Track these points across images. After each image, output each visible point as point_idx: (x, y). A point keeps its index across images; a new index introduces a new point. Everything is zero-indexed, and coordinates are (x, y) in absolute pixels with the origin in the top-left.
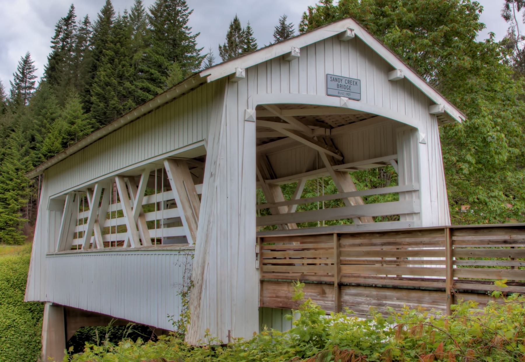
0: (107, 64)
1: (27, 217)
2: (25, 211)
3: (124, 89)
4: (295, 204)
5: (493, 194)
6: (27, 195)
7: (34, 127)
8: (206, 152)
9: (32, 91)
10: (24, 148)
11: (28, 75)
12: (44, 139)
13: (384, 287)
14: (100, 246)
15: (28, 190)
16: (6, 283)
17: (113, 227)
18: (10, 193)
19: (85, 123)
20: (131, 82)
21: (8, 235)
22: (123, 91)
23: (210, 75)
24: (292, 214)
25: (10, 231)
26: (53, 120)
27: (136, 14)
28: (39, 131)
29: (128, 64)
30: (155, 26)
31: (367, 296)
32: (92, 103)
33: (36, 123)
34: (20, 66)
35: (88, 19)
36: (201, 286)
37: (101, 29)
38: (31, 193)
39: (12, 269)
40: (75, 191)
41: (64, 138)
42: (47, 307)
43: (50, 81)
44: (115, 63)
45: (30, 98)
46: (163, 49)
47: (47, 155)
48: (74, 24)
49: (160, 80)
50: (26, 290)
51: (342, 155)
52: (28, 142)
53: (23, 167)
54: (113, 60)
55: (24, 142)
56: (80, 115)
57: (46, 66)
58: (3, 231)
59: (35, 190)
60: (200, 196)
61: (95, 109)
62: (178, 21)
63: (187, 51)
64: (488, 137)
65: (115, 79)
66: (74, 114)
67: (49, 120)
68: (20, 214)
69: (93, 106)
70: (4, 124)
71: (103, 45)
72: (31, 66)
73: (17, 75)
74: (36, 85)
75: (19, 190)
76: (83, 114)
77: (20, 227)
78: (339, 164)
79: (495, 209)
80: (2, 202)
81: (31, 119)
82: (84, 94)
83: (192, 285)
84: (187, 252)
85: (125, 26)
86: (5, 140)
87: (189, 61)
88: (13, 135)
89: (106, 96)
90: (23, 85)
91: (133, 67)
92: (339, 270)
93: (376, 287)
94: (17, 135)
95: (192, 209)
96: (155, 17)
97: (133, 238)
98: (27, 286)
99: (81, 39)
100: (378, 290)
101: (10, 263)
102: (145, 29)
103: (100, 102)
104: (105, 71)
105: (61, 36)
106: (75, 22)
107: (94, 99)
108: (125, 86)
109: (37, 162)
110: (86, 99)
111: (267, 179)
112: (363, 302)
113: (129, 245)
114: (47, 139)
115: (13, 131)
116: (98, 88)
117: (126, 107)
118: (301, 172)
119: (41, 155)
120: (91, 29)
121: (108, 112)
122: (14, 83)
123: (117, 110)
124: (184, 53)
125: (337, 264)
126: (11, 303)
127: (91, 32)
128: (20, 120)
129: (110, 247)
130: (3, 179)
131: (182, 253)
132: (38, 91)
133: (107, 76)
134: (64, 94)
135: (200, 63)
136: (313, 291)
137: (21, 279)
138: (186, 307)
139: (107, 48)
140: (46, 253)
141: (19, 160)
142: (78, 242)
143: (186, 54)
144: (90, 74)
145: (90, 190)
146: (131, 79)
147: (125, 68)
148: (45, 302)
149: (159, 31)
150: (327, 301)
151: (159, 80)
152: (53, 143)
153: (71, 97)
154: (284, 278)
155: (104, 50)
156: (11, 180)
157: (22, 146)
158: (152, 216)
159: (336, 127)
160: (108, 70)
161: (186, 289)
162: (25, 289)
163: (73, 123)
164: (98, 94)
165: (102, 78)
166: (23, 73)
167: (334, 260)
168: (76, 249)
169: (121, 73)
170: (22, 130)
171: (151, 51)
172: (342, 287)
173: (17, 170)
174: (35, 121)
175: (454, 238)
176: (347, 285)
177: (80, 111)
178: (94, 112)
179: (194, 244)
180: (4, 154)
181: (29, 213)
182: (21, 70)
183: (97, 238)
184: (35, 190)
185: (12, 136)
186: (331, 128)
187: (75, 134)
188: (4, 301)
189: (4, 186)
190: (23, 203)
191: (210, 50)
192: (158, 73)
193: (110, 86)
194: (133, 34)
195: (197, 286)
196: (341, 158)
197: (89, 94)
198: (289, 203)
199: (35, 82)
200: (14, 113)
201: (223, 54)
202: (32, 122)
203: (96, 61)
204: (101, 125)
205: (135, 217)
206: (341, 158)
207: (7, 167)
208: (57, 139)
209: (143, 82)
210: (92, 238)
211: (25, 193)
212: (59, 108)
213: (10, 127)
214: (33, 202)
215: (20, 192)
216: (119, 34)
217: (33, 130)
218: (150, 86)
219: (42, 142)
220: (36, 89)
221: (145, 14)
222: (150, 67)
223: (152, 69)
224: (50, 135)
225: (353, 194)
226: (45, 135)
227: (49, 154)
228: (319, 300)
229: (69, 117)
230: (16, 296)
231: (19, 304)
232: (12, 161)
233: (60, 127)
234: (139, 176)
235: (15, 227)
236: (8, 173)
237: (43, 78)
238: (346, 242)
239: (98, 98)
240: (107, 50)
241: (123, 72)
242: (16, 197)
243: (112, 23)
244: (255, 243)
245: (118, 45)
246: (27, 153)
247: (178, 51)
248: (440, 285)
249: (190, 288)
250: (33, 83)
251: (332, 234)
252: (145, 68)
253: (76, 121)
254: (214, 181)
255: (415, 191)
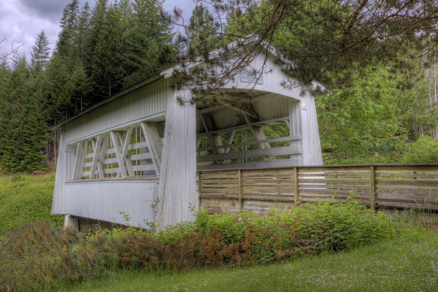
0: (103, 40)
1: (47, 154)
2: (45, 150)
3: (116, 58)
4: (228, 147)
5: (364, 137)
6: (46, 138)
7: (50, 88)
8: (165, 118)
9: (48, 59)
10: (43, 103)
11: (44, 48)
12: (58, 97)
13: (265, 200)
14: (102, 176)
15: (47, 134)
16: (38, 203)
17: (110, 164)
18: (34, 137)
19: (87, 84)
20: (121, 53)
21: (34, 167)
22: (115, 60)
23: (166, 73)
24: (226, 154)
25: (35, 165)
26: (64, 82)
27: (124, 2)
28: (54, 91)
29: (119, 40)
30: (138, 11)
31: (256, 206)
32: (93, 69)
33: (51, 85)
34: (37, 41)
35: (88, 5)
36: (163, 201)
37: (98, 13)
38: (50, 137)
39: (41, 192)
40: (84, 140)
41: (72, 96)
42: (67, 219)
43: (61, 52)
44: (109, 40)
45: (46, 64)
46: (144, 28)
47: (60, 108)
48: (78, 9)
49: (142, 51)
50: (52, 207)
51: (258, 116)
52: (47, 99)
53: (43, 118)
54: (108, 37)
55: (43, 99)
56: (84, 79)
57: (58, 41)
58: (30, 165)
59: (52, 134)
60: (163, 145)
61: (95, 74)
62: (155, 8)
63: (161, 30)
64: (358, 99)
65: (109, 52)
66: (79, 78)
67: (61, 82)
68: (42, 152)
69: (94, 71)
70: (28, 86)
71: (100, 25)
72: (45, 40)
73: (35, 48)
74: (50, 55)
75: (41, 134)
76: (86, 78)
77: (42, 162)
78: (255, 122)
79: (365, 146)
80: (28, 143)
81: (48, 81)
82: (86, 62)
83: (158, 201)
84: (156, 181)
85: (116, 12)
86: (29, 98)
87: (164, 37)
88: (35, 94)
89: (103, 64)
90: (40, 55)
91: (122, 42)
92: (242, 191)
93: (260, 200)
94: (38, 94)
95: (158, 153)
96: (138, 4)
97: (123, 171)
98: (53, 204)
99: (83, 20)
100: (262, 202)
101: (39, 188)
102: (131, 13)
103: (98, 68)
104: (101, 45)
105: (68, 18)
106: (78, 7)
107: (94, 66)
108: (116, 56)
109: (53, 114)
110: (88, 66)
111: (211, 130)
112: (254, 209)
113: (120, 176)
114: (60, 97)
115: (35, 91)
116: (97, 58)
117: (118, 72)
118: (232, 126)
119: (56, 109)
120: (90, 13)
121: (105, 76)
122: (33, 53)
123: (111, 75)
124: (160, 31)
125: (241, 187)
126: (41, 216)
127: (90, 14)
128: (39, 83)
129: (108, 177)
130: (29, 127)
131: (152, 181)
132: (52, 61)
133: (103, 49)
134: (72, 63)
135: (171, 39)
136: (228, 203)
137: (48, 199)
138: (155, 214)
139: (103, 28)
140: (65, 181)
141: (40, 113)
142: (86, 174)
143: (161, 32)
144: (91, 47)
145: (94, 139)
146: (121, 51)
147: (116, 43)
148: (65, 215)
149: (141, 15)
150: (236, 209)
151: (141, 52)
152: (65, 100)
153: (77, 65)
154: (213, 195)
155: (100, 30)
156: (35, 127)
157: (42, 102)
158: (134, 157)
159: (254, 97)
160: (104, 45)
161: (155, 203)
162: (51, 206)
163: (79, 85)
164: (97, 63)
165: (99, 51)
166: (40, 46)
167: (239, 185)
168: (85, 178)
169: (113, 47)
170: (41, 90)
171: (135, 30)
172: (244, 201)
173: (39, 120)
174: (50, 83)
175: (299, 173)
176: (245, 199)
177: (84, 75)
178: (94, 76)
179: (159, 176)
180: (28, 108)
181: (48, 151)
182: (38, 44)
183: (99, 171)
184: (52, 134)
185: (34, 94)
186: (251, 98)
187: (81, 93)
188: (37, 215)
189: (30, 132)
190: (44, 144)
191: (178, 30)
192: (141, 47)
193: (106, 56)
194: (122, 17)
195: (161, 201)
196: (257, 117)
197: (90, 63)
198: (225, 146)
199: (49, 52)
200: (35, 77)
201: (188, 32)
202: (48, 84)
203: (94, 38)
204: (99, 86)
205: (123, 158)
206: (257, 117)
207: (31, 118)
208: (68, 97)
209: (129, 53)
210: (96, 171)
211: (45, 136)
212: (68, 74)
213: (32, 88)
214: (51, 143)
215: (41, 136)
216: (111, 18)
217: (49, 90)
218: (135, 56)
219: (57, 99)
220: (50, 58)
221: (130, 3)
222: (135, 42)
223: (136, 43)
224: (62, 93)
225: (263, 141)
226: (59, 94)
227: (62, 108)
228: (231, 208)
229: (76, 80)
230: (45, 211)
231: (47, 216)
232: (35, 113)
233: (69, 88)
234: (127, 131)
235: (38, 162)
236: (32, 122)
237: (55, 50)
238: (245, 174)
239: (97, 66)
240: (103, 30)
241: (115, 46)
242: (39, 140)
243: (106, 9)
244: (196, 175)
245: (111, 26)
246: (45, 107)
247: (155, 30)
248: (290, 199)
249: (157, 202)
250: (47, 54)
251: (238, 170)
252: (131, 43)
253: (81, 83)
254: (170, 138)
255: (299, 140)
